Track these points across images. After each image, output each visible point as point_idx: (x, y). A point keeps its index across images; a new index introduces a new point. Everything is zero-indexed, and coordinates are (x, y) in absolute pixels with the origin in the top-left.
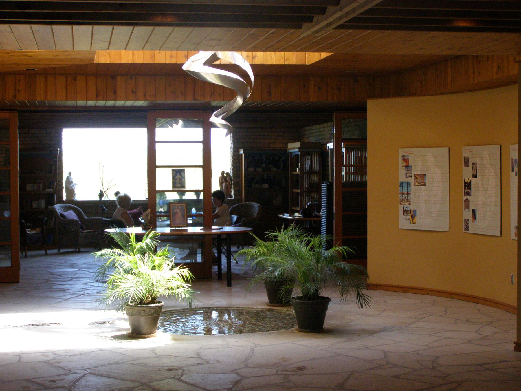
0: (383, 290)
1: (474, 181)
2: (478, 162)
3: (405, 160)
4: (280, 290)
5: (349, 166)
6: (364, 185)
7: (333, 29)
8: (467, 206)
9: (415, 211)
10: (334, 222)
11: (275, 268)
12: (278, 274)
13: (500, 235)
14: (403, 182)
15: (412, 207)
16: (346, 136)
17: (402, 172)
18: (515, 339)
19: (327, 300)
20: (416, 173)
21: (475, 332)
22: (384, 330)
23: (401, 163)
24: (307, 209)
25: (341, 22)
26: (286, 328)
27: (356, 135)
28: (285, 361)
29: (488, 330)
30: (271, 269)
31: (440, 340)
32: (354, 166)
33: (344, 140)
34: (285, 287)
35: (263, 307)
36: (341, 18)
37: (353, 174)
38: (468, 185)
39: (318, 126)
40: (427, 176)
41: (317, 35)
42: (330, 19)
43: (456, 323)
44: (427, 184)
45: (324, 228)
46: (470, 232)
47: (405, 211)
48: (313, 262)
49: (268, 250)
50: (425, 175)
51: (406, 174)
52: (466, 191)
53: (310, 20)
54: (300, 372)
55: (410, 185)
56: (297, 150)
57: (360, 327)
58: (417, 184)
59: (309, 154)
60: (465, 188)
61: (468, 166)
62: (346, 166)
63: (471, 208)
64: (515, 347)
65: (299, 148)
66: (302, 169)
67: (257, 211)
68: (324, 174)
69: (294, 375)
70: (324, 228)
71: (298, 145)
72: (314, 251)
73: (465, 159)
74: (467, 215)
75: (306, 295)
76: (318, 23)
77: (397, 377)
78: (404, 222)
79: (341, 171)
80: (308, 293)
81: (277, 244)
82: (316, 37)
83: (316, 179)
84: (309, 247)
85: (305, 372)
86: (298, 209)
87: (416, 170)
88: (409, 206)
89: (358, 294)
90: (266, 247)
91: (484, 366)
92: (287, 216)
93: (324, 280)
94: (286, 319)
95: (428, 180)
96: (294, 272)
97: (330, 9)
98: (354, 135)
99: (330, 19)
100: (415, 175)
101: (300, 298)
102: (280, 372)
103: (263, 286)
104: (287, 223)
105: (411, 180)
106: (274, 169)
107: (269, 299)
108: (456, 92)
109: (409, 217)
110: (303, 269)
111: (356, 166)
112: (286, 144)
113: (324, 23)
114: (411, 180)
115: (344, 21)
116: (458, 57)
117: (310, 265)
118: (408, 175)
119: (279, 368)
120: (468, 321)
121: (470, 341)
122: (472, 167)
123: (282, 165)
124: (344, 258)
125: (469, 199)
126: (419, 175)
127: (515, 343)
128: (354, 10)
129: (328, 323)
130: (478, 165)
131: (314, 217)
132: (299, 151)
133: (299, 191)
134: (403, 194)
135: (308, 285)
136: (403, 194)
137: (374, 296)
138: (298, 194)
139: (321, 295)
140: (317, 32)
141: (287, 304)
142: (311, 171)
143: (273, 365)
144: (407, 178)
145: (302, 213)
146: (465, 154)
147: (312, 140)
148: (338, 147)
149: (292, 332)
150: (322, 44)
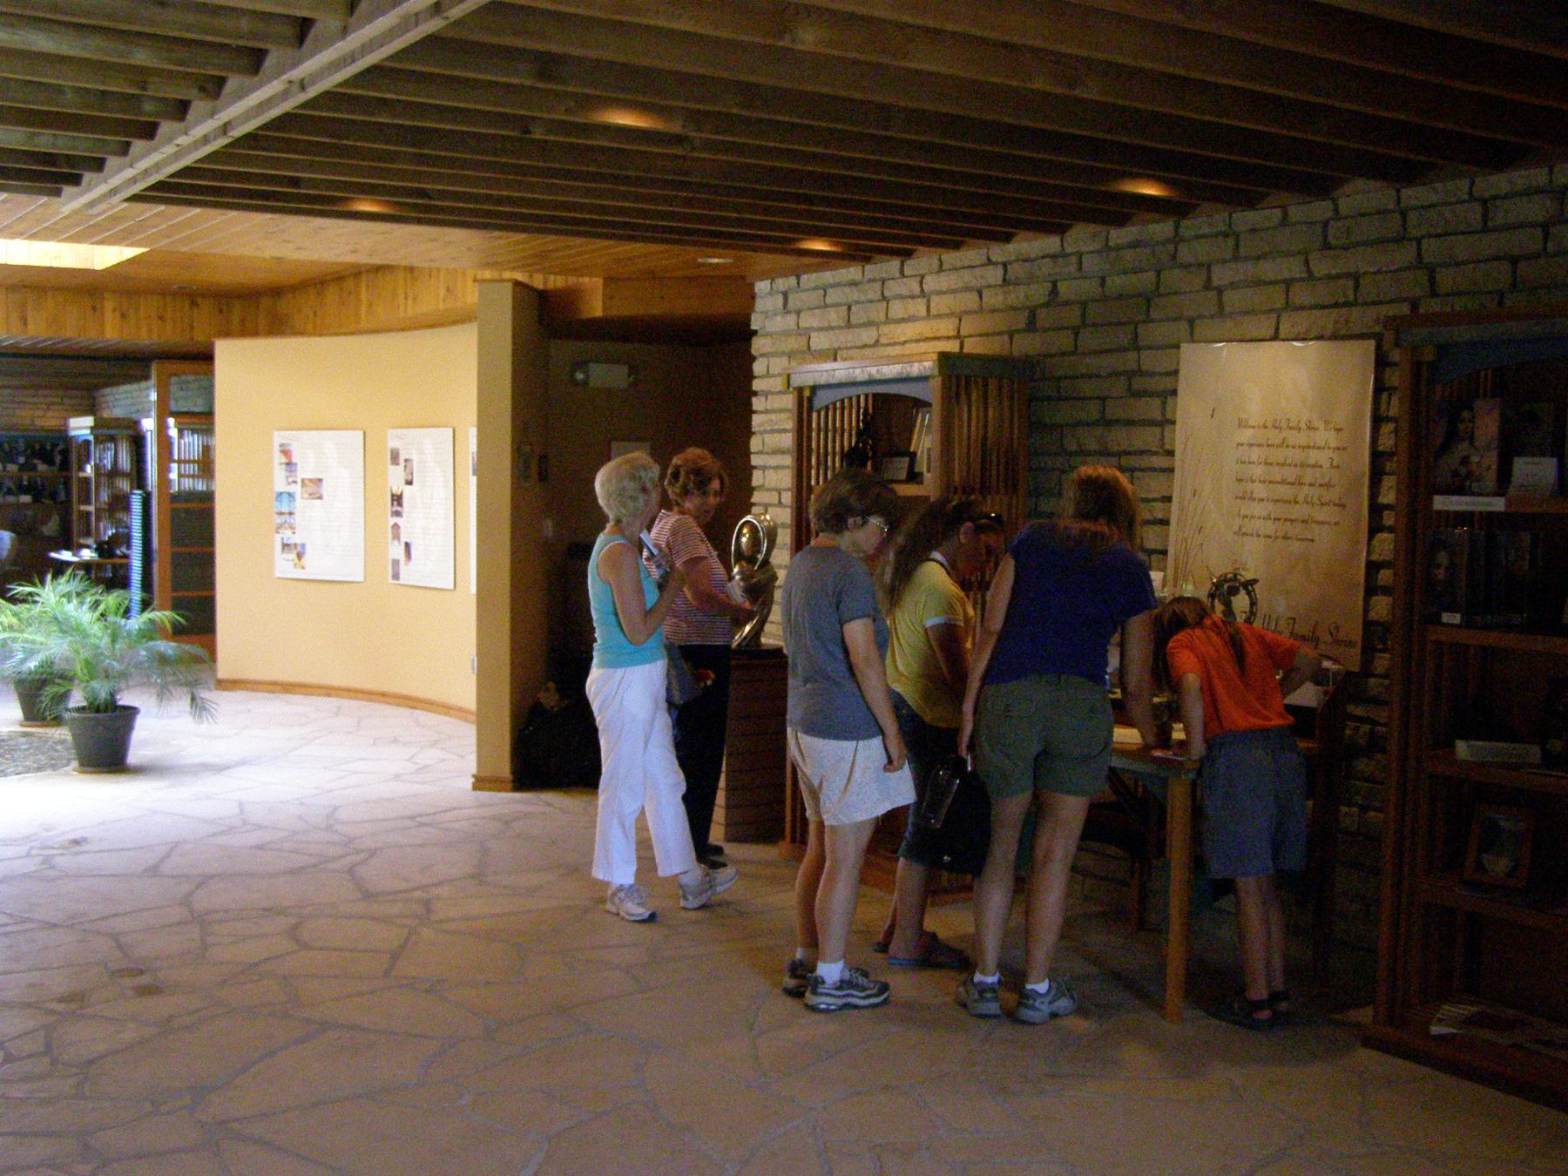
0: (247, 689)
1: (407, 490)
2: (415, 457)
3: (286, 453)
4: (40, 696)
5: (185, 462)
6: (208, 498)
7: (125, 200)
8: (396, 536)
9: (303, 546)
10: (156, 566)
11: (30, 653)
12: (35, 666)
13: (452, 587)
14: (281, 494)
15: (296, 539)
16: (174, 407)
17: (280, 473)
18: (474, 770)
19: (130, 713)
20: (304, 476)
21: (407, 760)
22: (242, 763)
23: (279, 459)
24: (107, 543)
25: (137, 188)
26: (54, 767)
27: (198, 406)
28: (46, 830)
29: (430, 756)
30: (20, 656)
31: (342, 778)
32: (194, 462)
33: (173, 414)
34: (50, 690)
35: (12, 729)
36: (134, 180)
37: (193, 476)
38: (397, 499)
39: (127, 387)
40: (324, 481)
41: (94, 211)
42: (115, 182)
43: (374, 744)
44: (325, 497)
45: (136, 577)
46: (402, 581)
47: (286, 546)
48: (107, 640)
49: (19, 620)
50: (320, 480)
51: (287, 477)
52: (395, 509)
53: (75, 180)
54: (77, 849)
55: (293, 497)
56: (88, 431)
57: (197, 761)
58: (306, 496)
59: (112, 439)
60: (392, 504)
61: (398, 464)
62: (179, 462)
63: (403, 539)
64: (474, 784)
65: (92, 428)
66: (97, 468)
67: (9, 547)
68: (139, 478)
69: (62, 855)
70: (136, 577)
71: (89, 421)
72: (106, 620)
73: (392, 452)
74: (397, 551)
75: (91, 703)
76: (90, 188)
77: (260, 847)
78: (284, 565)
79: (169, 470)
80: (95, 699)
81: (38, 609)
82: (92, 216)
83: (124, 485)
84: (98, 613)
85: (85, 847)
86: (90, 541)
87: (305, 471)
88: (292, 536)
89: (193, 699)
90: (15, 615)
91: (418, 819)
92: (66, 555)
93: (124, 675)
94: (57, 751)
95: (326, 489)
96: (67, 660)
97: (112, 162)
98: (195, 405)
99: (115, 182)
100: (303, 481)
101: (83, 709)
102: (34, 852)
103: (12, 687)
104: (60, 568)
105: (297, 489)
106: (42, 467)
107: (25, 714)
108: (378, 331)
109: (293, 556)
110: (85, 654)
111: (198, 462)
112: (66, 419)
113: (103, 189)
114: (297, 489)
115: (142, 188)
116: (379, 269)
117: (98, 647)
118: (290, 480)
119: (35, 843)
120: (395, 741)
121: (397, 777)
122: (405, 467)
123: (58, 459)
124: (178, 632)
125: (399, 524)
126: (311, 480)
127: (474, 776)
128: (157, 167)
129: (134, 756)
130: (415, 463)
131: (120, 557)
132: (92, 433)
133: (91, 508)
134: (281, 514)
135: (95, 684)
136: (281, 514)
137: (225, 704)
138: (88, 514)
139: (121, 703)
140: (92, 204)
141: (57, 721)
142: (115, 472)
143: (23, 839)
144: (289, 484)
145: (96, 550)
146: (393, 443)
147: (118, 412)
148: (162, 428)
149: (67, 774)
150: (108, 230)
